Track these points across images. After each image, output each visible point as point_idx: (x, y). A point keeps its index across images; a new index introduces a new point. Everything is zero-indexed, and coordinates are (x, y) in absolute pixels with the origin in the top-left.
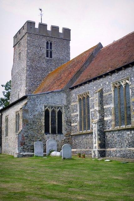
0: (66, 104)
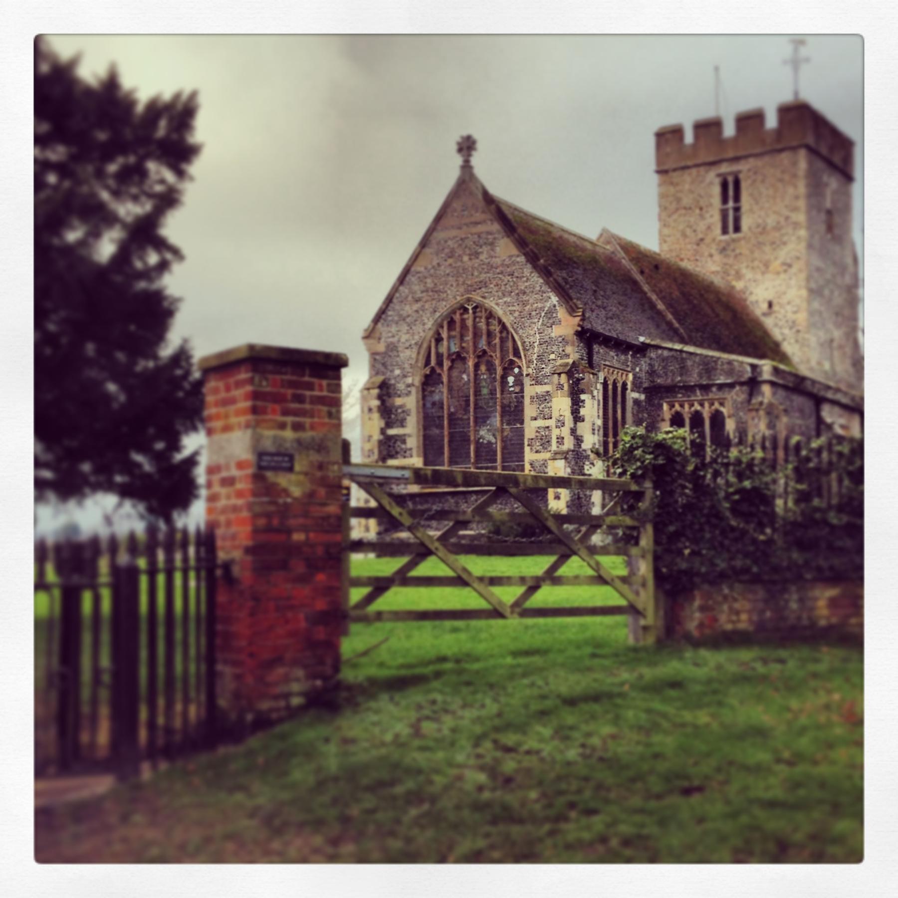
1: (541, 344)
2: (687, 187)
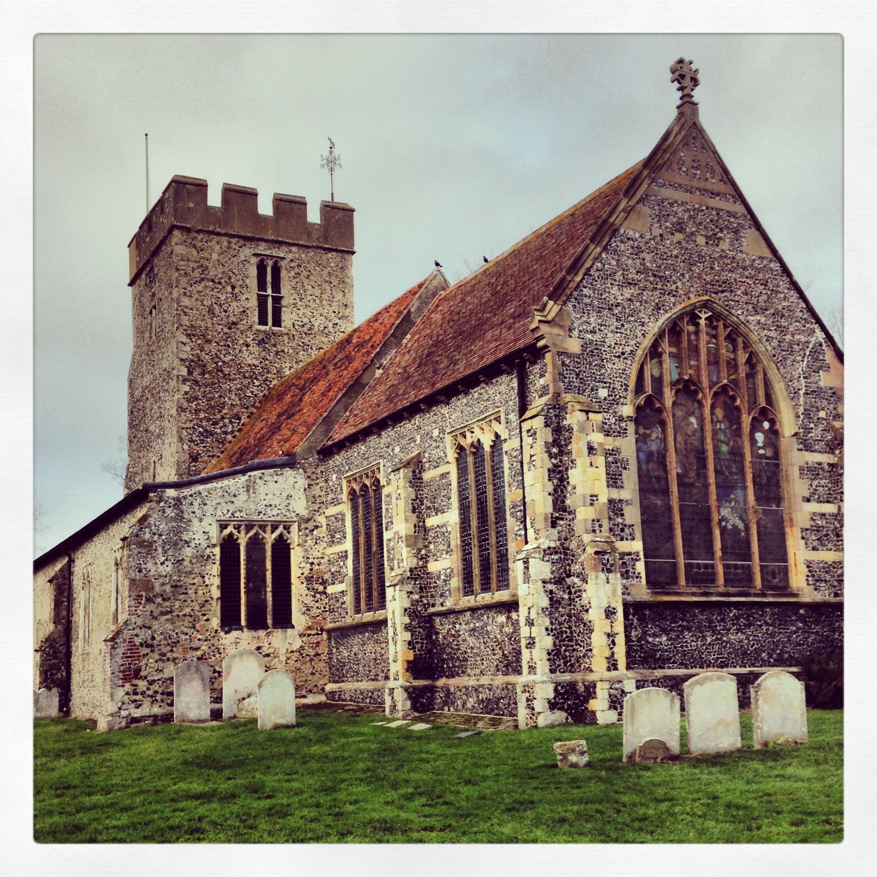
0: (304, 513)
1: (808, 394)
2: (215, 256)
